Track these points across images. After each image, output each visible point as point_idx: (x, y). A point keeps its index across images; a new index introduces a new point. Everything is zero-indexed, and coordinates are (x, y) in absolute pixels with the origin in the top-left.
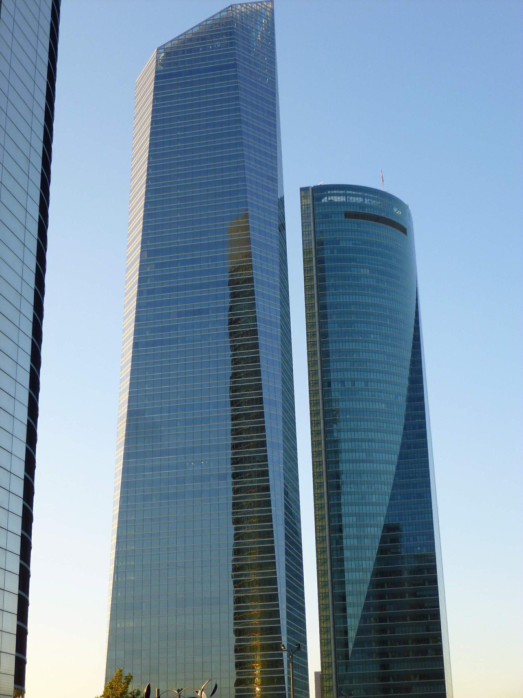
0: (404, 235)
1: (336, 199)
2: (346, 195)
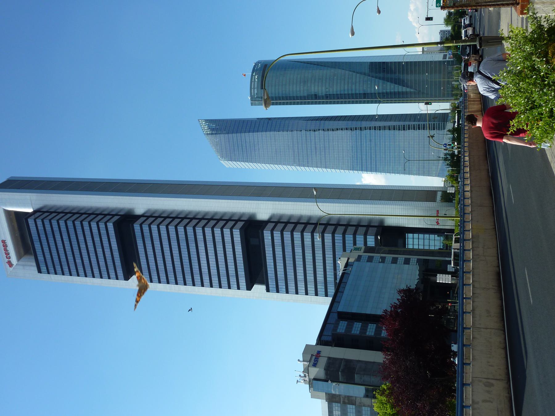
0: (268, 65)
1: (256, 92)
2: (254, 89)
